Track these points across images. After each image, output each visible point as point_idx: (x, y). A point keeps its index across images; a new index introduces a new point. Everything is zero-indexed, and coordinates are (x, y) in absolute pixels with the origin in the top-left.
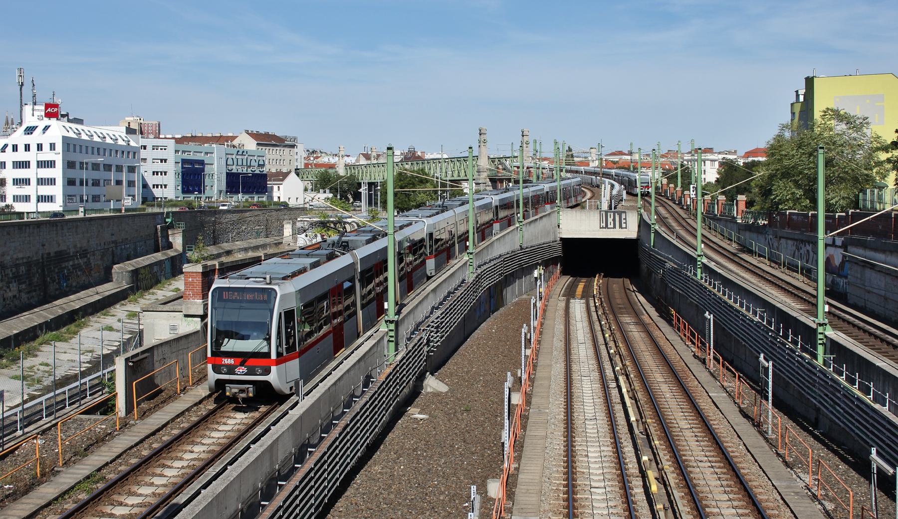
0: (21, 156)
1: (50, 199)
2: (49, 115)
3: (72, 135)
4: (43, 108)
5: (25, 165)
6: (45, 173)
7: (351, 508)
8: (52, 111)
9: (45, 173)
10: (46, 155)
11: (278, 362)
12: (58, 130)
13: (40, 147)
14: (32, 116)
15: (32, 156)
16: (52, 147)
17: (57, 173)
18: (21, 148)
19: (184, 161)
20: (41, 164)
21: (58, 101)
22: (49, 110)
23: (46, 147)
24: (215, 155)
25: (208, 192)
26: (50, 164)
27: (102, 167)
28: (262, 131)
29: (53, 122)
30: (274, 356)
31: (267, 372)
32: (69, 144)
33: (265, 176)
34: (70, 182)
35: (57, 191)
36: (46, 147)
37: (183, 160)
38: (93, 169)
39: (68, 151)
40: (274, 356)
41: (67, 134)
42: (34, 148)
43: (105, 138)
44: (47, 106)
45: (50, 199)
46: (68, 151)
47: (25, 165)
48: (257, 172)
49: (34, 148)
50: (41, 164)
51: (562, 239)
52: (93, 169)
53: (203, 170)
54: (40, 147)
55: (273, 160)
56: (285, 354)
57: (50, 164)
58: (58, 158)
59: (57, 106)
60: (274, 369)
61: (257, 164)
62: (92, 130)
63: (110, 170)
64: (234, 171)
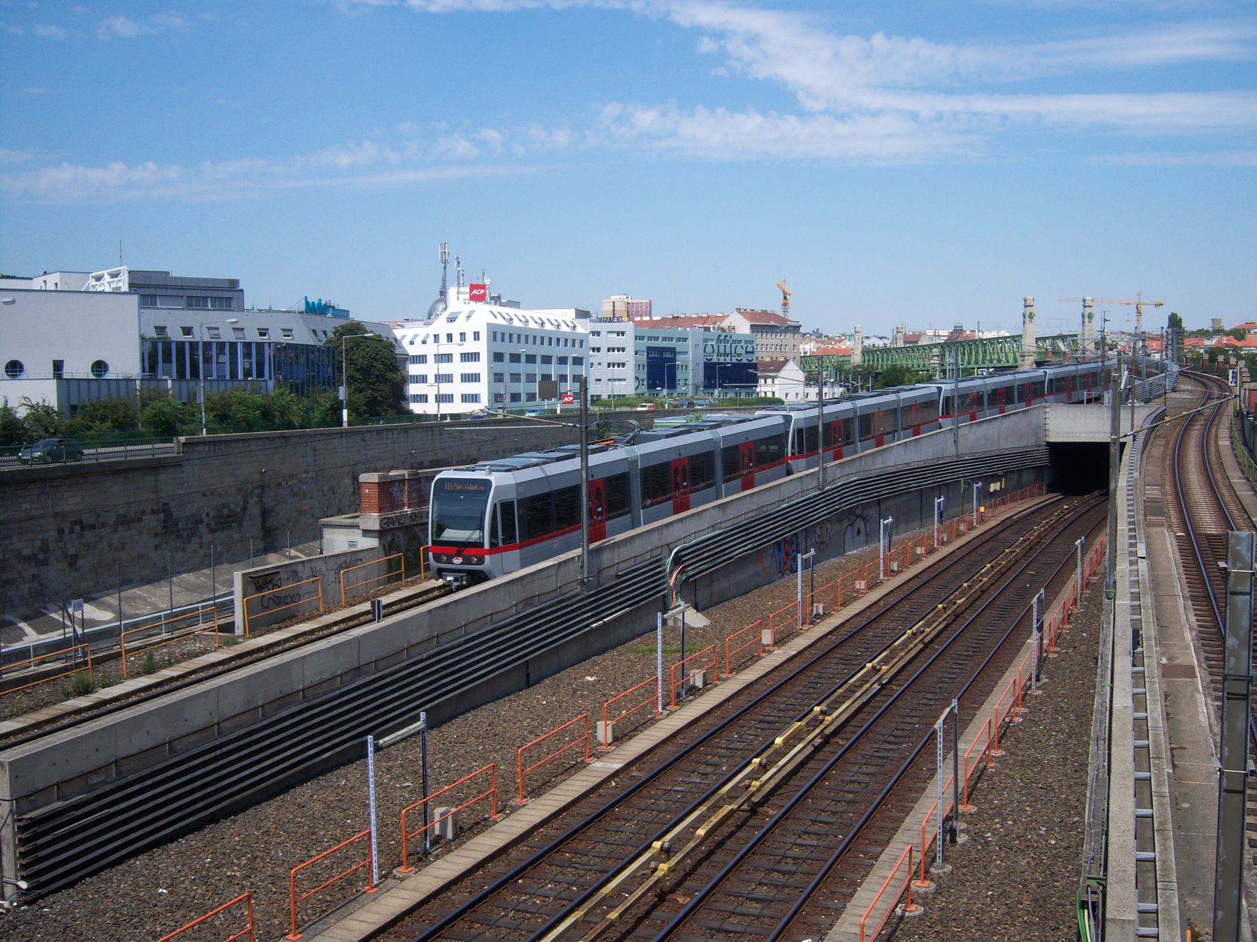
0: (445, 349)
1: (475, 398)
2: (474, 298)
3: (500, 321)
4: (467, 290)
5: (447, 358)
6: (471, 368)
7: (1041, 903)
8: (478, 294)
9: (471, 368)
10: (470, 346)
11: (490, 552)
12: (484, 316)
13: (463, 335)
14: (457, 300)
15: (455, 349)
16: (477, 336)
17: (481, 367)
18: (443, 338)
19: (650, 349)
20: (466, 357)
21: (487, 282)
22: (475, 292)
23: (470, 337)
24: (690, 342)
25: (681, 388)
26: (474, 357)
27: (523, 359)
28: (758, 309)
29: (479, 306)
30: (487, 546)
31: (481, 561)
32: (496, 334)
33: (754, 366)
34: (498, 377)
35: (482, 388)
36: (470, 337)
37: (649, 348)
38: (511, 361)
39: (495, 339)
40: (487, 546)
41: (494, 321)
42: (456, 338)
43: (543, 324)
44: (473, 287)
45: (475, 398)
46: (495, 339)
47: (447, 358)
48: (744, 361)
49: (456, 338)
50: (466, 357)
51: (1049, 444)
52: (511, 361)
53: (674, 360)
54: (463, 335)
55: (766, 349)
56: (501, 544)
57: (474, 357)
58: (482, 347)
59: (483, 287)
60: (487, 557)
61: (743, 351)
62: (528, 314)
63: (566, 363)
64: (715, 359)
